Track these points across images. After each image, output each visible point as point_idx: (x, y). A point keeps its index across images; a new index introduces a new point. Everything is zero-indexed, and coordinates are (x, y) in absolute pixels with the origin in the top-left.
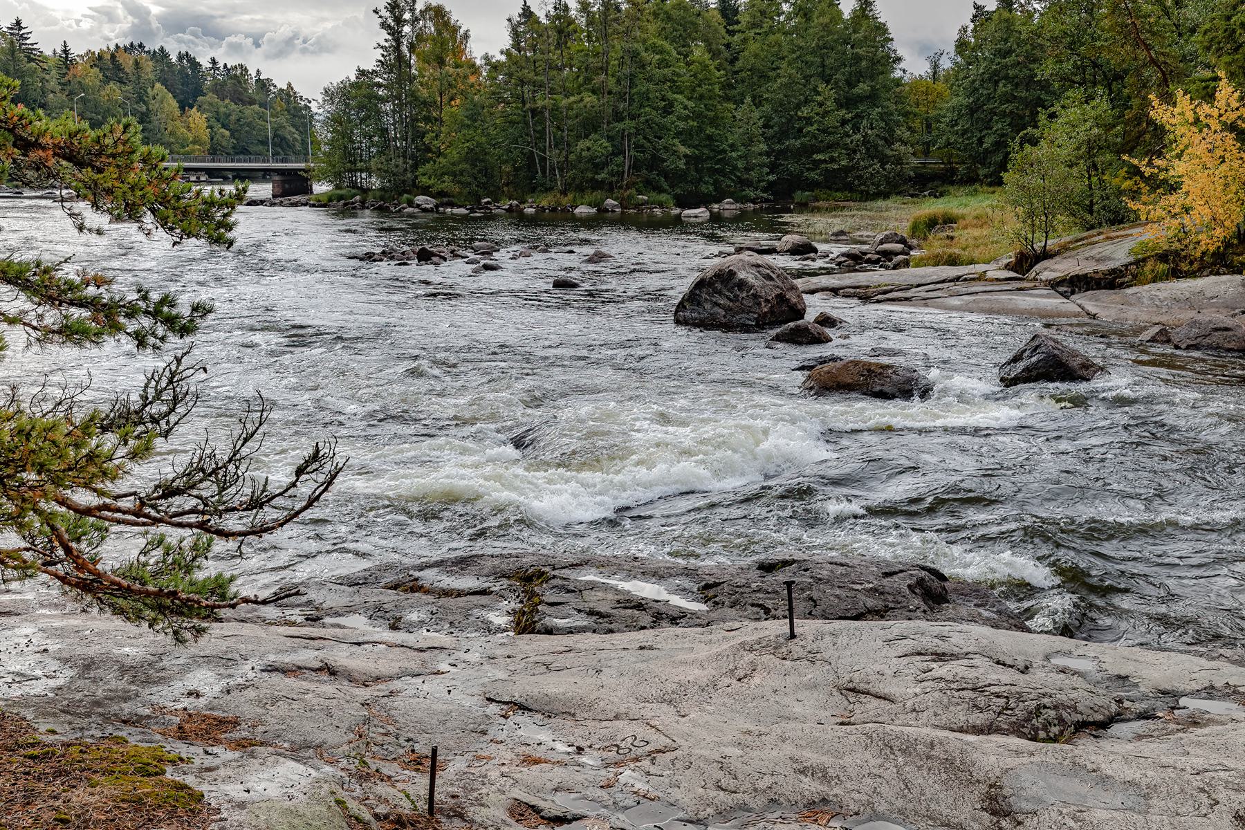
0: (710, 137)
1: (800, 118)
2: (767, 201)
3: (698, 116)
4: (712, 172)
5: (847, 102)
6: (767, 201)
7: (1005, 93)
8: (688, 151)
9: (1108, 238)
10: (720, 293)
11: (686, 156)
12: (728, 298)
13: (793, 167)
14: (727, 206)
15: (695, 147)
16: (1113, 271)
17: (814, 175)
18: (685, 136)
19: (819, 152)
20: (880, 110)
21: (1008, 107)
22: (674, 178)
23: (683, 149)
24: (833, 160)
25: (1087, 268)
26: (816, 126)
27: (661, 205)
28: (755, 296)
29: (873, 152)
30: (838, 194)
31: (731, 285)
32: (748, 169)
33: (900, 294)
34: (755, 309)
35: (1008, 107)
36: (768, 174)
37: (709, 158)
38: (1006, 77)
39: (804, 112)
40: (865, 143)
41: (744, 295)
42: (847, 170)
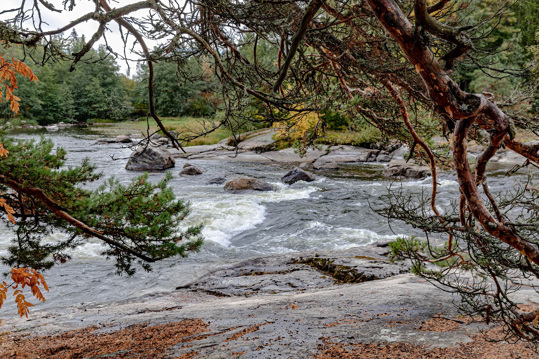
0: (50, 97)
1: (86, 91)
2: (76, 123)
3: (45, 88)
4: (52, 111)
5: (104, 85)
6: (76, 123)
7: (165, 84)
8: (43, 103)
9: (260, 134)
10: (146, 157)
11: (41, 105)
12: (150, 159)
13: (85, 110)
14: (61, 125)
15: (45, 101)
16: (269, 145)
17: (93, 113)
18: (40, 96)
19: (95, 104)
20: (117, 88)
21: (165, 89)
22: (36, 113)
23: (40, 102)
24: (101, 107)
25: (260, 144)
26: (93, 94)
27: (32, 124)
28: (162, 158)
29: (115, 104)
30: (104, 120)
31: (150, 154)
32: (67, 111)
33: (197, 156)
34: (162, 163)
35: (165, 89)
36: (75, 112)
37: (51, 106)
38: (165, 78)
39: (88, 88)
40: (113, 101)
41: (157, 158)
42: (106, 111)
